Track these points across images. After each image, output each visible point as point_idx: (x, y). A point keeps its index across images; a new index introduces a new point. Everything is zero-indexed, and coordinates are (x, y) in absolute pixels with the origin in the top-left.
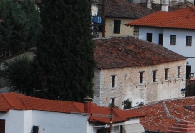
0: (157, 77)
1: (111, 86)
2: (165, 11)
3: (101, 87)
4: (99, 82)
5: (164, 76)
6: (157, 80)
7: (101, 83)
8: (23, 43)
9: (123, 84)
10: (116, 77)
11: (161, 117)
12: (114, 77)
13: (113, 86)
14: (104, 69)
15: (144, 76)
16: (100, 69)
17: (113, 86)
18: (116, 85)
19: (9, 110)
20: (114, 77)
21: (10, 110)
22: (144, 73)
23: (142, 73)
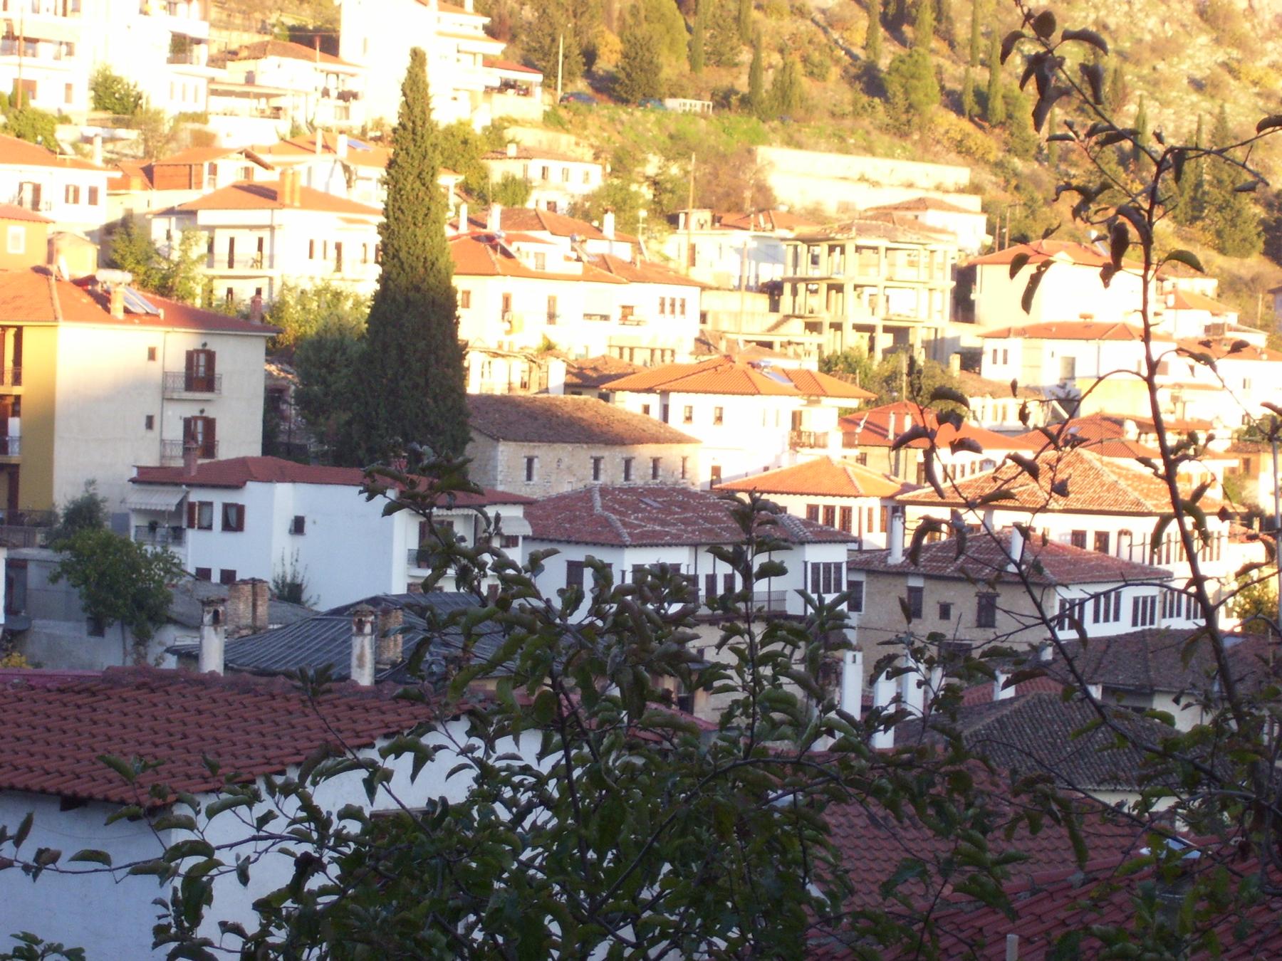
0: (633, 471)
1: (524, 478)
2: (377, 591)
3: (500, 478)
4: (495, 468)
5: (651, 471)
6: (633, 477)
7: (500, 469)
8: (1016, 160)
9: (553, 478)
10: (536, 460)
11: (351, 906)
12: (530, 461)
13: (529, 477)
14: (505, 439)
15: (602, 466)
16: (497, 440)
17: (529, 477)
18: (535, 478)
19: (245, 483)
20: (530, 461)
21: (249, 484)
22: (602, 461)
23: (597, 461)
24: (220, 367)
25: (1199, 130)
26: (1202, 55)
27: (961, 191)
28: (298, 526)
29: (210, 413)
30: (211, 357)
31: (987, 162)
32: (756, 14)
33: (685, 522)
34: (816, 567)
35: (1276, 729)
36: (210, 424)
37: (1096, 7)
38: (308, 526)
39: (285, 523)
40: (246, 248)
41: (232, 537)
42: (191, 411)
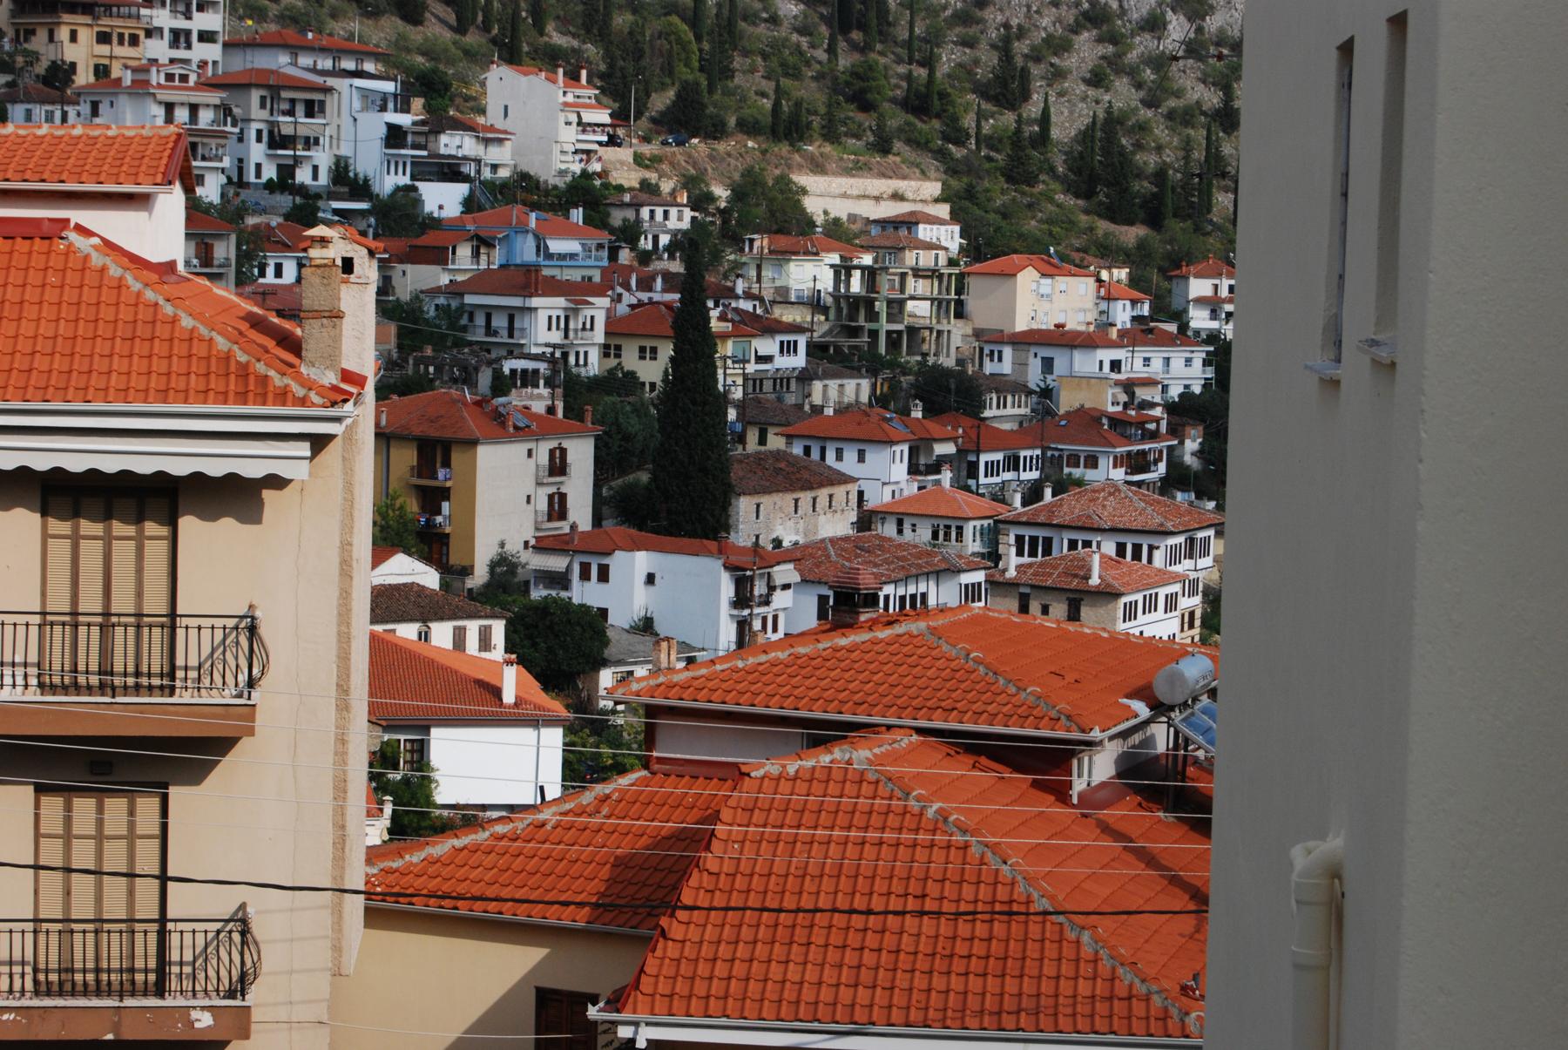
12: (758, 506)
20: (758, 506)
23: (797, 501)
24: (569, 459)
25: (1094, 122)
26: (1087, 50)
27: (937, 201)
28: (650, 579)
29: (563, 490)
30: (563, 451)
31: (931, 151)
32: (742, 25)
33: (886, 561)
34: (967, 586)
35: (1007, 426)
36: (563, 497)
37: (1001, 10)
38: (657, 580)
39: (642, 577)
40: (500, 322)
41: (603, 586)
42: (553, 490)
